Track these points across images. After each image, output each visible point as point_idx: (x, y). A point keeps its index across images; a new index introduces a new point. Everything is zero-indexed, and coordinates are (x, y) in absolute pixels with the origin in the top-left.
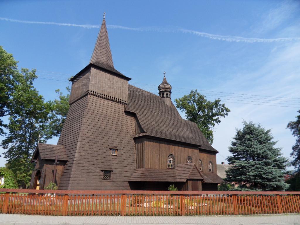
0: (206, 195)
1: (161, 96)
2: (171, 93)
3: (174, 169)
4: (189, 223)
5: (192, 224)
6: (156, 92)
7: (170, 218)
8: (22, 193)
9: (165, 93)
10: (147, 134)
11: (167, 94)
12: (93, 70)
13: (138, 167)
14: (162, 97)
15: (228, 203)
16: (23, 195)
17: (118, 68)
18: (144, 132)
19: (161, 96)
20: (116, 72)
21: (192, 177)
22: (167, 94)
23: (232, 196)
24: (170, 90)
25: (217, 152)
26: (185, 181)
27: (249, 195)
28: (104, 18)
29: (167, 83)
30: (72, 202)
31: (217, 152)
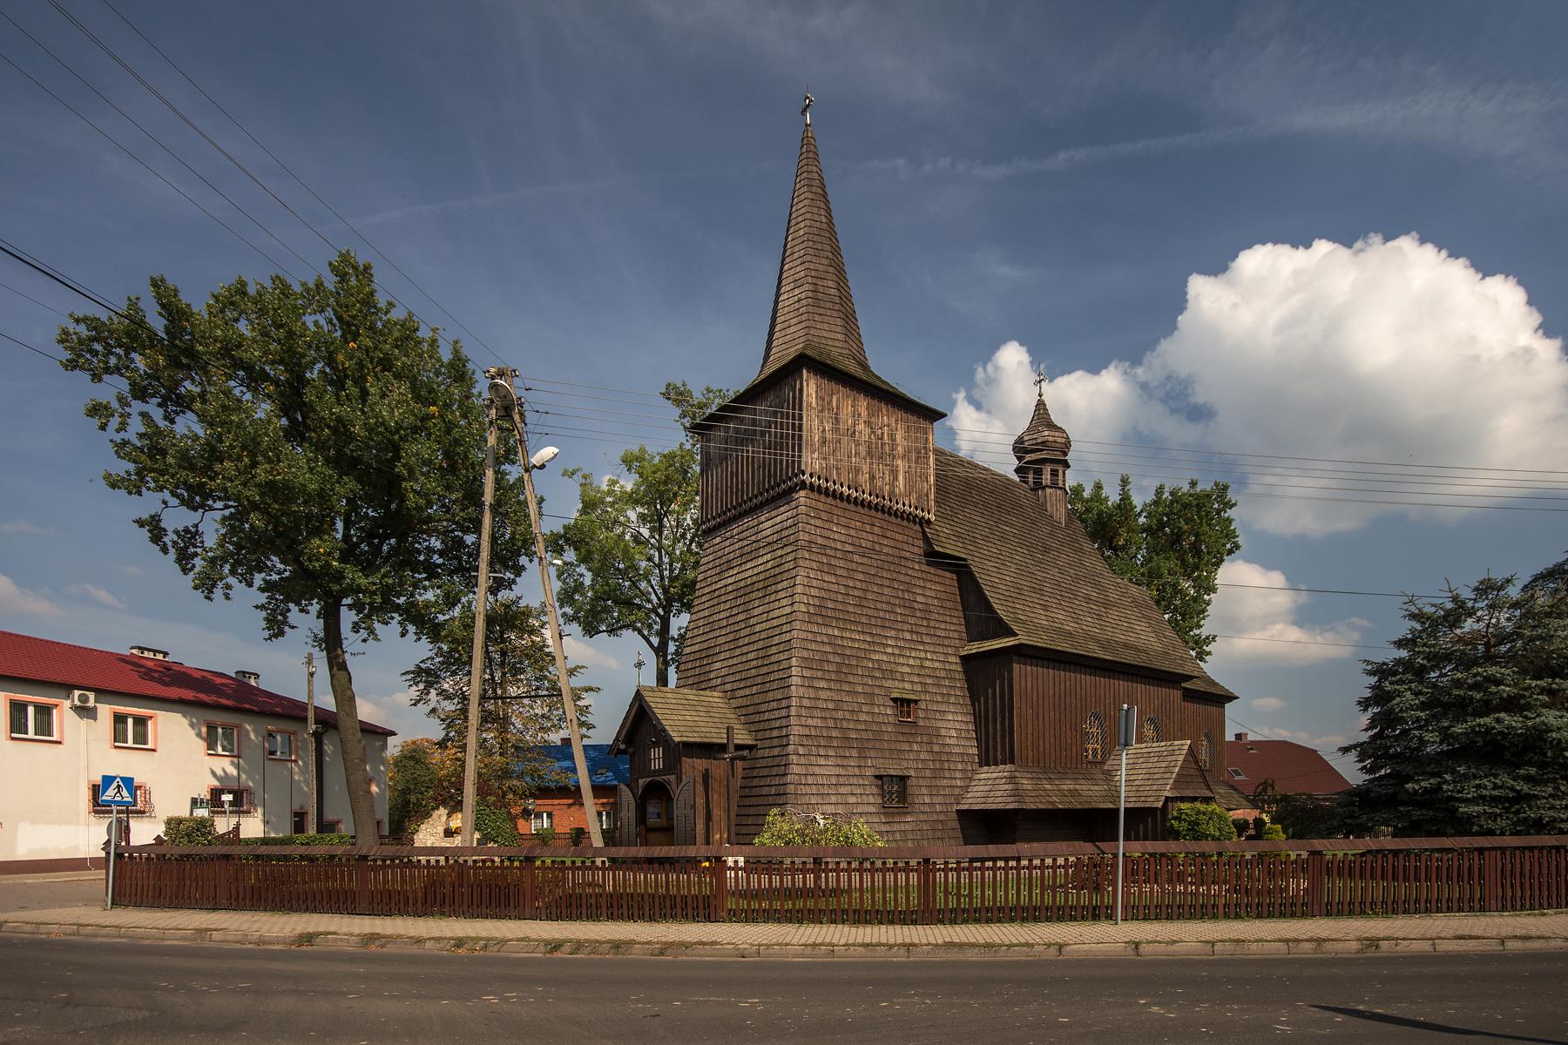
0: (443, 858)
1: (1027, 483)
2: (1066, 465)
3: (1103, 763)
4: (1070, 942)
5: (1193, 944)
6: (1007, 466)
7: (981, 930)
8: (428, 858)
9: (1047, 470)
10: (1023, 638)
11: (1054, 473)
12: (810, 387)
13: (986, 759)
14: (1031, 483)
15: (1372, 878)
16: (578, 864)
17: (886, 367)
18: (1011, 633)
19: (1027, 483)
20: (878, 383)
21: (698, 785)
22: (1054, 473)
23: (1486, 853)
24: (1065, 454)
25: (1231, 698)
26: (1160, 805)
27: (1408, 853)
28: (809, 122)
29: (1051, 426)
30: (830, 880)
31: (1231, 698)
